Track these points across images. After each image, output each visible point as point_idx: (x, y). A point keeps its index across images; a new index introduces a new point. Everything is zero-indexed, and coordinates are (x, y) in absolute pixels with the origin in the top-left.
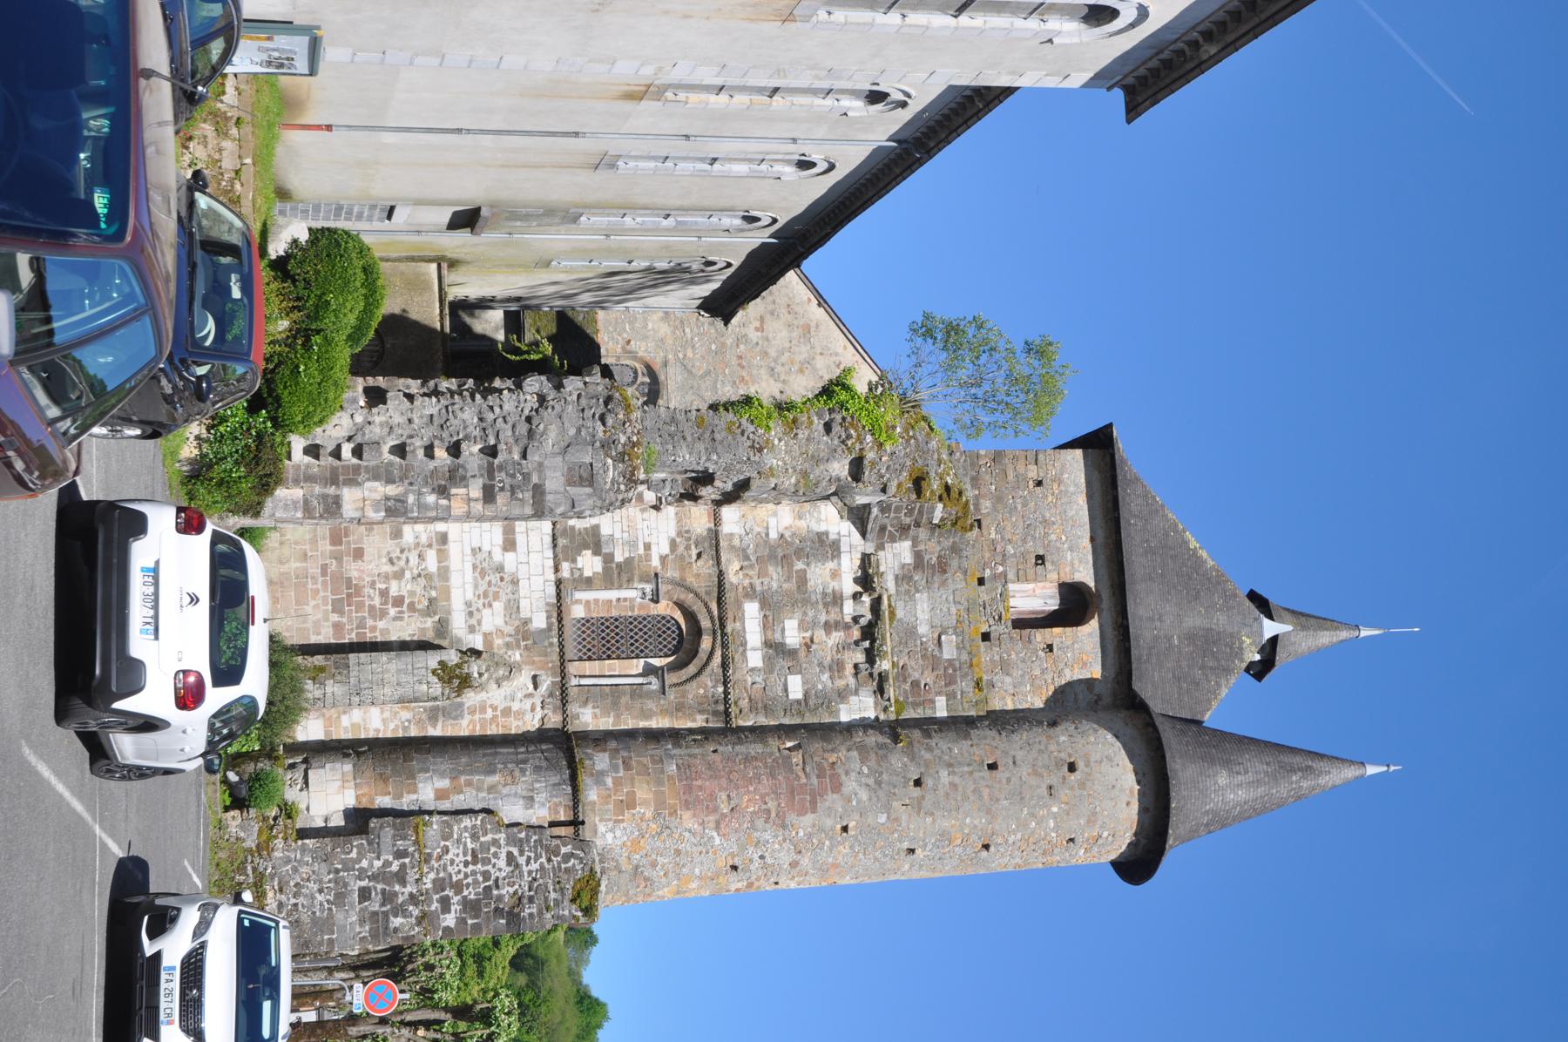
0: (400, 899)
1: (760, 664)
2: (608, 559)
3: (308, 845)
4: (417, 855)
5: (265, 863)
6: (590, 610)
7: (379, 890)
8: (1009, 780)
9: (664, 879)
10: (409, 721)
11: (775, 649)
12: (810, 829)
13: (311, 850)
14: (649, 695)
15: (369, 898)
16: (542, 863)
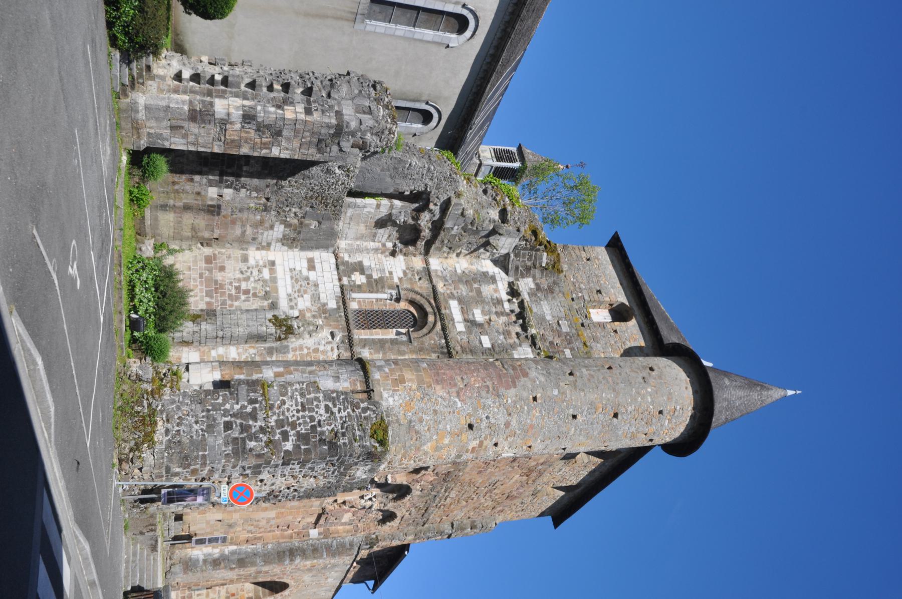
0: (253, 430)
1: (464, 330)
2: (369, 277)
4: (264, 403)
5: (157, 403)
6: (361, 305)
8: (620, 374)
9: (428, 434)
10: (255, 354)
11: (471, 323)
12: (514, 398)
14: (402, 343)
15: (231, 428)
16: (348, 413)
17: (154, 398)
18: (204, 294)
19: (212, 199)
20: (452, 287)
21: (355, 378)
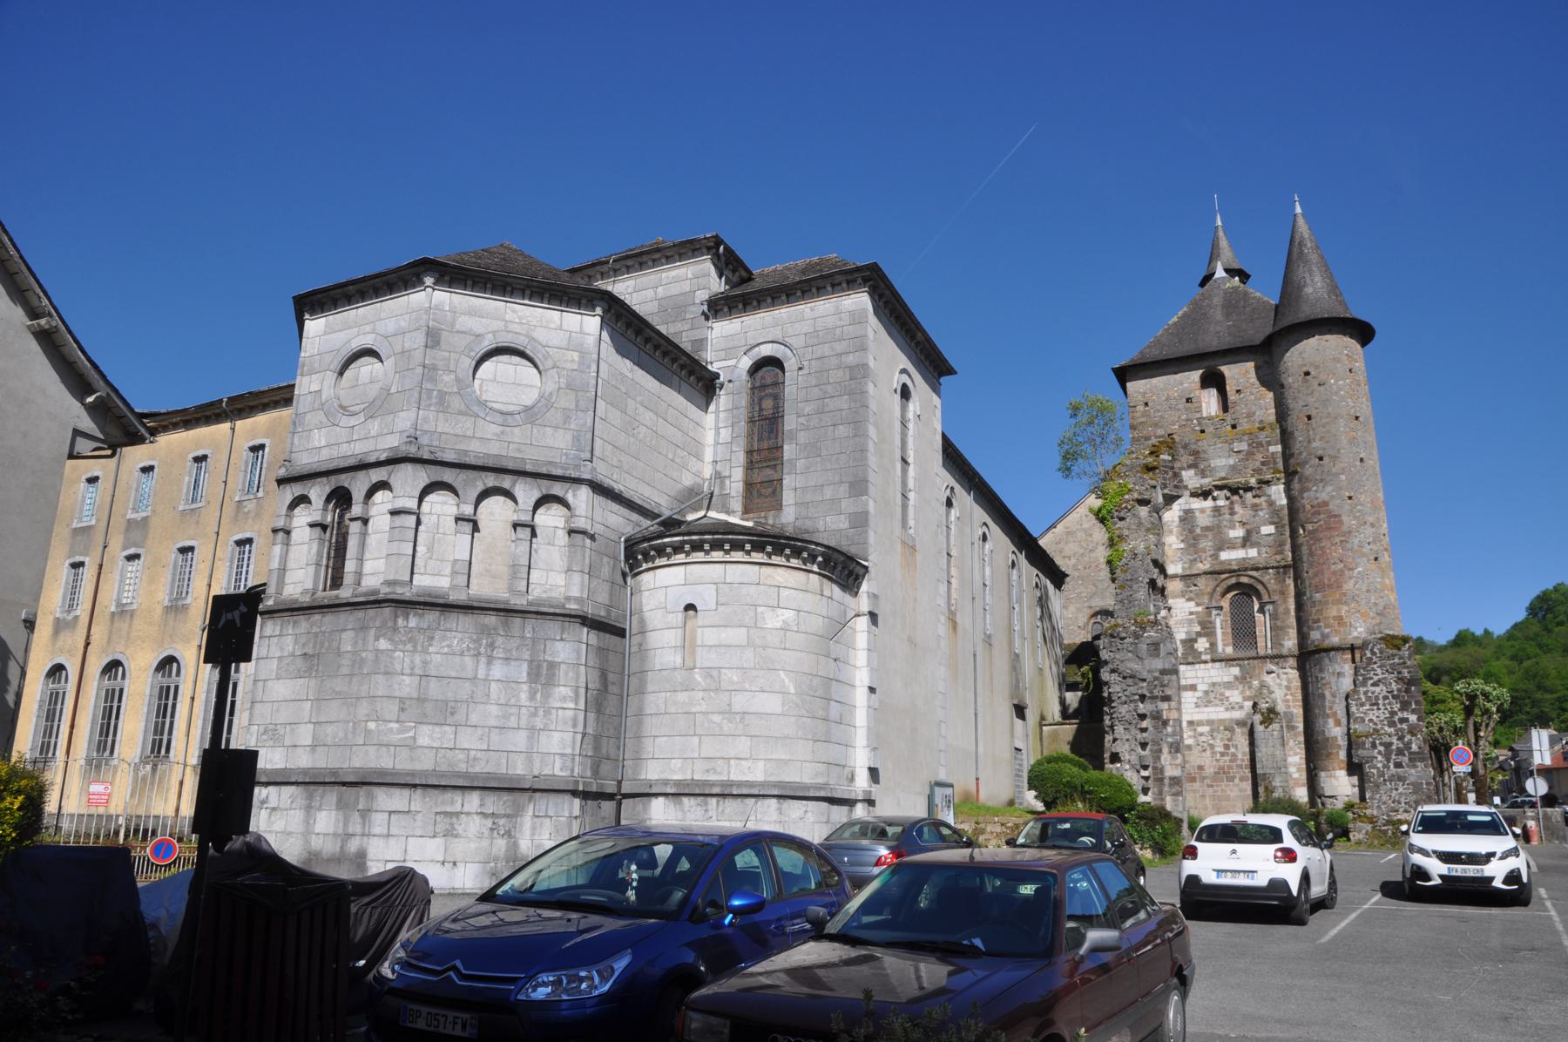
0: (1401, 745)
1: (1255, 550)
2: (1199, 634)
11: (1246, 542)
14: (1275, 610)
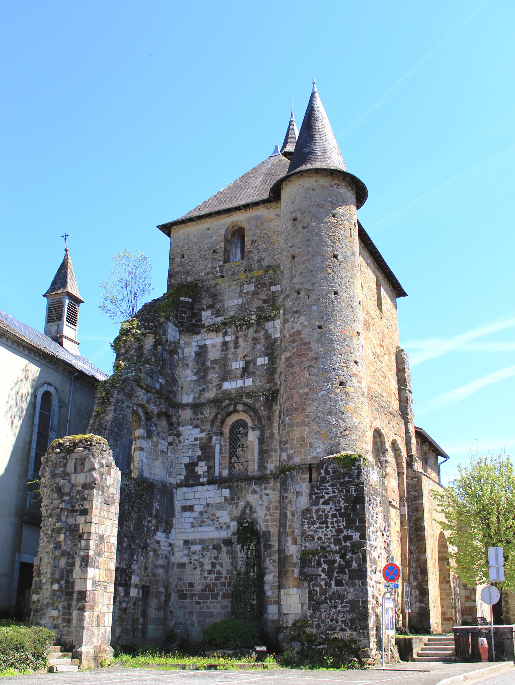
0: (343, 563)
1: (251, 379)
3: (311, 614)
6: (225, 467)
7: (337, 575)
10: (270, 560)
11: (245, 372)
13: (314, 613)
16: (329, 486)
17: (315, 640)
18: (215, 600)
19: (138, 593)
20: (211, 386)
21: (299, 479)
